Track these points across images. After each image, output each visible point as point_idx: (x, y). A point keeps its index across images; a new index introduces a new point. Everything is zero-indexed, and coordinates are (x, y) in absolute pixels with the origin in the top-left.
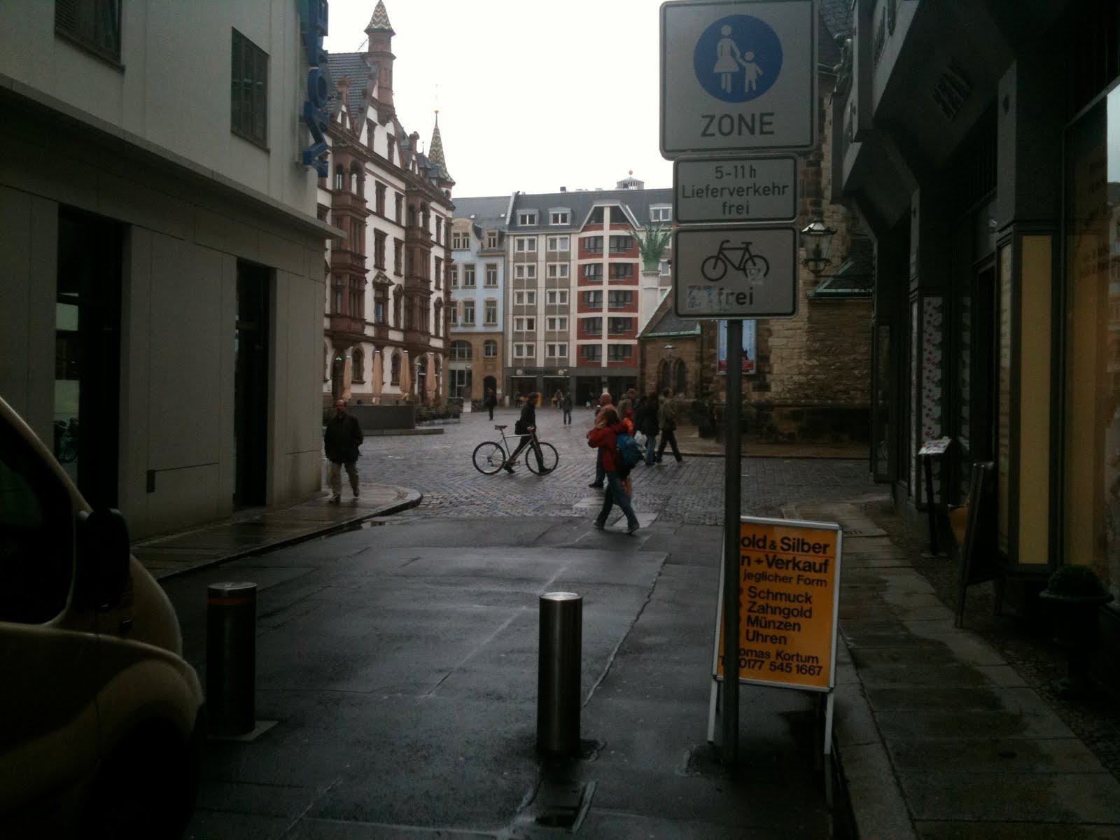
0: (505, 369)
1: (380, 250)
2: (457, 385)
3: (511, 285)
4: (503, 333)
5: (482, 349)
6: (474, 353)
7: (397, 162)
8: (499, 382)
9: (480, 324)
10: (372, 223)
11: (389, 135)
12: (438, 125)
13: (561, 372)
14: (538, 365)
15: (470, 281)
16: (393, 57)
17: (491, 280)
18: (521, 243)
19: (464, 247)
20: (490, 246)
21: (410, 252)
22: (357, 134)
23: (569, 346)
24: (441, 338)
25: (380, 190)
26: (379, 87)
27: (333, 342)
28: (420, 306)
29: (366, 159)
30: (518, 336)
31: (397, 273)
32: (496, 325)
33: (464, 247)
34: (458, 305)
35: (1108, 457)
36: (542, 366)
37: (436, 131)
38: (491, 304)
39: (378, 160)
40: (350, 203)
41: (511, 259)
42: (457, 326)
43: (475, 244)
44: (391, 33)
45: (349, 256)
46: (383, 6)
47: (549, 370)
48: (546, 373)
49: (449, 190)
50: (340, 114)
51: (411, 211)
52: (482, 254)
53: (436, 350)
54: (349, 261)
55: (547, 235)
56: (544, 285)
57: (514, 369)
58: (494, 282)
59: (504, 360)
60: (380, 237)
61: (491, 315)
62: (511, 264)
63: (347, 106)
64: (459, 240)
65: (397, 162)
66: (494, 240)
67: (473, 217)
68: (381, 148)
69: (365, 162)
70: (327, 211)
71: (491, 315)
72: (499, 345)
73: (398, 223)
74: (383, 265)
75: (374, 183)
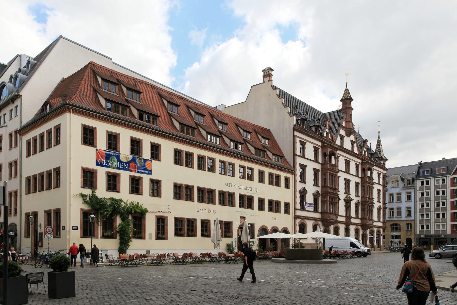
0: (415, 234)
1: (348, 187)
3: (418, 211)
4: (414, 220)
5: (405, 228)
6: (401, 229)
7: (356, 151)
8: (413, 240)
9: (404, 216)
10: (342, 176)
11: (351, 141)
13: (443, 236)
14: (431, 233)
15: (399, 200)
16: (352, 109)
17: (409, 198)
18: (422, 183)
20: (408, 185)
21: (363, 187)
22: (335, 140)
23: (447, 225)
24: (320, 213)
25: (347, 163)
26: (346, 122)
29: (337, 149)
30: (421, 221)
31: (357, 196)
32: (411, 217)
34: (394, 209)
35: (71, 195)
36: (434, 233)
38: (409, 209)
39: (346, 151)
40: (329, 167)
41: (418, 189)
42: (394, 217)
43: (401, 184)
45: (329, 188)
47: (437, 235)
48: (436, 236)
49: (385, 162)
50: (364, 151)
51: (364, 170)
52: (404, 188)
53: (378, 227)
54: (329, 191)
55: (435, 178)
56: (433, 199)
57: (420, 235)
58: (410, 199)
59: (415, 232)
60: (347, 182)
61: (409, 214)
62: (418, 192)
63: (329, 130)
65: (356, 151)
66: (410, 182)
67: (401, 174)
68: (347, 145)
69: (337, 151)
70: (319, 171)
71: (409, 214)
72: (413, 225)
73: (357, 176)
74: (349, 193)
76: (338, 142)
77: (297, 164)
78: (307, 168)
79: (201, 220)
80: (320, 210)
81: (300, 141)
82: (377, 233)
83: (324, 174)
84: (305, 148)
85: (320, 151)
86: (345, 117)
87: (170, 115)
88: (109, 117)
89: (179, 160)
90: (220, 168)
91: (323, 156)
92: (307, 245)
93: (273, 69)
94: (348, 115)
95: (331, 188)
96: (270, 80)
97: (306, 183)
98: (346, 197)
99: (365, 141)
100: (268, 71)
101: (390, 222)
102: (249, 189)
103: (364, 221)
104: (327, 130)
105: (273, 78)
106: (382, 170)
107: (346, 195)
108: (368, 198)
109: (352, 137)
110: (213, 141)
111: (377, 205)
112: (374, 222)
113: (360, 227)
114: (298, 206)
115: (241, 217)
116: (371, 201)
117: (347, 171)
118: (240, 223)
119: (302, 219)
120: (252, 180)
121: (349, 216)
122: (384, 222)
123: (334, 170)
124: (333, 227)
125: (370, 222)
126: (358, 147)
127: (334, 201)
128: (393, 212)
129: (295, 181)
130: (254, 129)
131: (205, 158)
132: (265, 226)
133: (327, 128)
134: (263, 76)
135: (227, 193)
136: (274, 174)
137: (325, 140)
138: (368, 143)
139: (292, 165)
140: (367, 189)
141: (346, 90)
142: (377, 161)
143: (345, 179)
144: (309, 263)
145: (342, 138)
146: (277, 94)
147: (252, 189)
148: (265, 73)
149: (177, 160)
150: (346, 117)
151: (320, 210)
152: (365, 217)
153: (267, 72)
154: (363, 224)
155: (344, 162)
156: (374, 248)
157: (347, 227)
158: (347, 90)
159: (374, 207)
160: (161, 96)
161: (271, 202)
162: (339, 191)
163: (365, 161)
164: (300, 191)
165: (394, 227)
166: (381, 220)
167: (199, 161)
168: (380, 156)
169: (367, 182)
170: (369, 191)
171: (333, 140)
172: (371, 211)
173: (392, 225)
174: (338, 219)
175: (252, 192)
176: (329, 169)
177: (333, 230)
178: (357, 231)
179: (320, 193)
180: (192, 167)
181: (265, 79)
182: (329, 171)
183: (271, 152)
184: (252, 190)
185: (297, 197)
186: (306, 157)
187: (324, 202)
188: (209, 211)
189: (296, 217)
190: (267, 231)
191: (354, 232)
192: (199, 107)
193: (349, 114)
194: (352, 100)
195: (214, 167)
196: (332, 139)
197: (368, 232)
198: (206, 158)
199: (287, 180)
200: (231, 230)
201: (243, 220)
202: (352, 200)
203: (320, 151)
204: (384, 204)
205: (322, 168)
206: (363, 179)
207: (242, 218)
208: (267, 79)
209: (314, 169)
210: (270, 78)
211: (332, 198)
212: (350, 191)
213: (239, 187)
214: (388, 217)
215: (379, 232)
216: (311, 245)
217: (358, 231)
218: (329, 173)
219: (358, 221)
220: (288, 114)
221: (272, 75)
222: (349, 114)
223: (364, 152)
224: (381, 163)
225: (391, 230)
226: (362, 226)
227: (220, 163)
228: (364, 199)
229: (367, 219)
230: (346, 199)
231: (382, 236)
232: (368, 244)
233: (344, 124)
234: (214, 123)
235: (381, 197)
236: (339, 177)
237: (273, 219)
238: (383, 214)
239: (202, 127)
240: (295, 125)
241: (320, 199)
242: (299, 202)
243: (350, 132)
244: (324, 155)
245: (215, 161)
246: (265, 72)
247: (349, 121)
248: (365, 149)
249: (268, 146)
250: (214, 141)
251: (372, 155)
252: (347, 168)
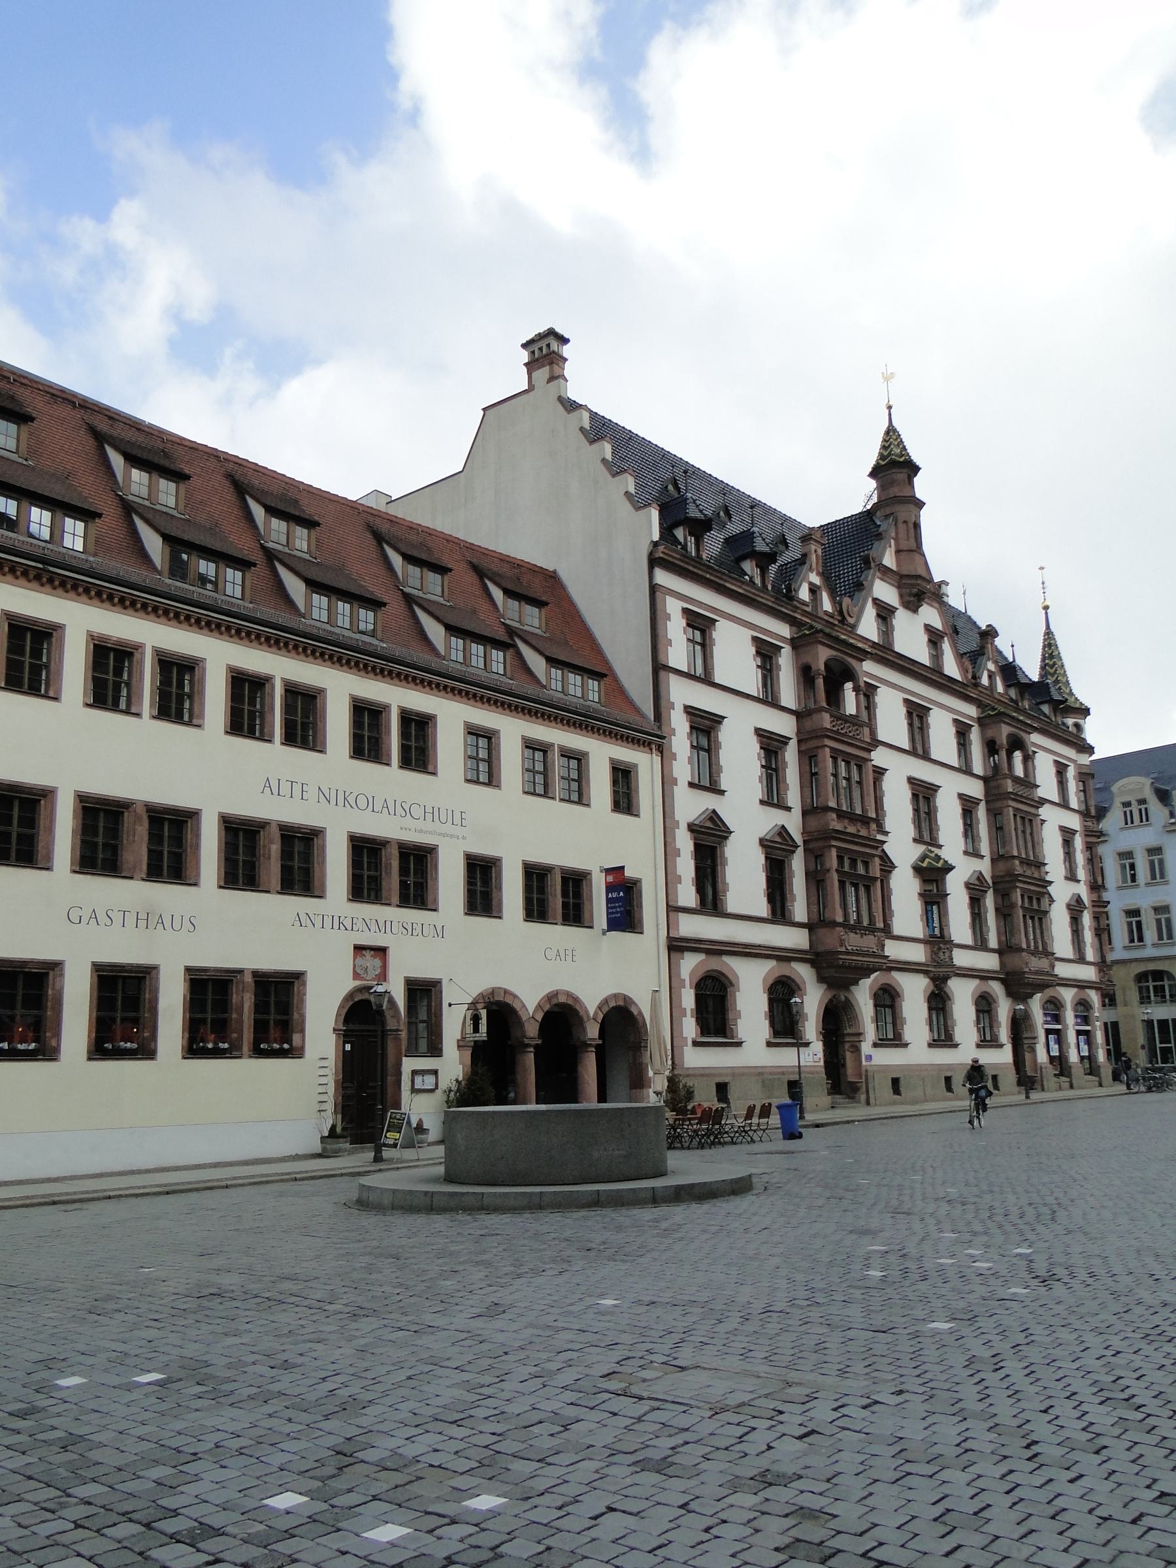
2: (1158, 1045)
7: (951, 668)
11: (928, 629)
12: (1052, 627)
16: (920, 504)
19: (1142, 821)
21: (994, 814)
24: (993, 951)
25: (917, 714)
27: (1007, 989)
28: (837, 870)
33: (1142, 821)
34: (1143, 912)
37: (1049, 634)
40: (1010, 790)
44: (912, 469)
45: (834, 816)
46: (895, 431)
53: (1081, 985)
64: (1131, 812)
65: (951, 668)
69: (1030, 733)
75: (901, 703)
76: (868, 627)
77: (672, 706)
78: (940, 791)
79: (98, 968)
80: (800, 910)
81: (686, 611)
82: (1075, 1010)
83: (810, 758)
84: (875, 707)
85: (975, 736)
86: (893, 535)
87: (409, 600)
88: (40, 566)
89: (180, 702)
90: (528, 770)
91: (802, 680)
92: (743, 1074)
93: (566, 336)
94: (902, 527)
95: (841, 815)
96: (552, 378)
97: (722, 793)
98: (923, 858)
99: (990, 633)
100: (543, 344)
101: (1134, 964)
102: (408, 812)
103: (1015, 961)
104: (815, 579)
105: (569, 370)
106: (1070, 752)
107: (921, 849)
108: (1021, 863)
109: (930, 615)
110: (474, 663)
111: (1061, 892)
112: (1057, 963)
113: (997, 988)
114: (687, 895)
115: (359, 949)
116: (1036, 875)
117: (919, 748)
118: (356, 976)
119: (708, 952)
120: (431, 769)
121: (942, 936)
122: (1103, 965)
123: (853, 738)
124: (871, 988)
125: (1036, 963)
126: (960, 656)
127: (861, 870)
128: (1139, 924)
129: (668, 782)
130: (475, 561)
131: (137, 656)
132: (506, 992)
133: (811, 570)
134: (526, 364)
135: (276, 834)
136: (552, 745)
137: (805, 613)
138: (1001, 643)
139: (650, 713)
140: (1010, 823)
141: (887, 433)
142: (1048, 717)
143: (911, 781)
144: (537, 1205)
145: (885, 613)
146: (582, 429)
147: (429, 809)
148: (533, 352)
149: (105, 688)
150: (897, 534)
151: (800, 910)
152: (1014, 941)
153: (541, 349)
154: (1007, 974)
155: (904, 711)
156: (1069, 1076)
157: (936, 986)
158: (891, 433)
159: (1052, 901)
160: (379, 538)
161: (535, 876)
162: (887, 830)
163: (993, 709)
164: (692, 828)
165: (1151, 984)
166: (1090, 955)
167: (405, 734)
168: (1057, 697)
169: (1007, 796)
170: (1024, 832)
171: (842, 618)
172: (1039, 916)
173: (1141, 977)
174: (888, 951)
175: (428, 825)
176: (824, 734)
177: (871, 1003)
178: (984, 1006)
179: (798, 838)
180: (51, 694)
181: (535, 374)
182: (828, 742)
183: (541, 653)
184: (429, 816)
185: (678, 853)
186: (718, 680)
187: (815, 879)
188: (149, 919)
189: (677, 946)
190: (519, 1018)
191: (924, 1007)
192: (180, 448)
193: (905, 522)
194: (916, 469)
195: (196, 698)
196: (841, 612)
197: (1036, 1005)
198: (143, 654)
199: (623, 775)
200: (296, 1016)
201: (371, 963)
202: (949, 868)
203: (975, 736)
204: (1096, 886)
205: (799, 733)
206: (993, 784)
207: (368, 954)
208: (542, 374)
209: (961, 796)
210: (551, 371)
211: (853, 862)
212: (938, 830)
213: (351, 799)
214: (1121, 946)
215: (1083, 1006)
216: (760, 1074)
217: (989, 1004)
218: (827, 750)
219: (989, 962)
220: (624, 499)
221: (565, 360)
222: (905, 522)
223: (990, 677)
224: (1064, 724)
225: (1142, 998)
226: (1004, 982)
227: (529, 752)
228: (1002, 866)
229: (1023, 950)
230: (925, 865)
231: (1098, 1024)
232: (1039, 1060)
233: (889, 560)
234: (249, 517)
235: (1080, 858)
236: (880, 772)
237: (551, 954)
238: (1096, 929)
239: (438, 613)
240: (655, 544)
241: (797, 864)
242: (693, 874)
243: (915, 591)
244: (991, 747)
245: (204, 670)
246: (536, 347)
247: (913, 547)
248: (991, 666)
249: (538, 632)
250: (559, 684)
251: (1027, 688)
252: (918, 737)
